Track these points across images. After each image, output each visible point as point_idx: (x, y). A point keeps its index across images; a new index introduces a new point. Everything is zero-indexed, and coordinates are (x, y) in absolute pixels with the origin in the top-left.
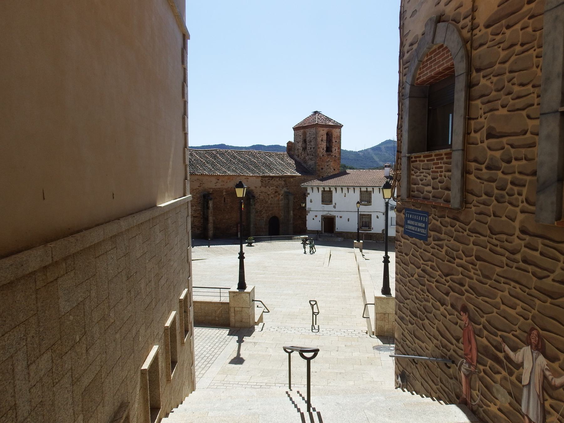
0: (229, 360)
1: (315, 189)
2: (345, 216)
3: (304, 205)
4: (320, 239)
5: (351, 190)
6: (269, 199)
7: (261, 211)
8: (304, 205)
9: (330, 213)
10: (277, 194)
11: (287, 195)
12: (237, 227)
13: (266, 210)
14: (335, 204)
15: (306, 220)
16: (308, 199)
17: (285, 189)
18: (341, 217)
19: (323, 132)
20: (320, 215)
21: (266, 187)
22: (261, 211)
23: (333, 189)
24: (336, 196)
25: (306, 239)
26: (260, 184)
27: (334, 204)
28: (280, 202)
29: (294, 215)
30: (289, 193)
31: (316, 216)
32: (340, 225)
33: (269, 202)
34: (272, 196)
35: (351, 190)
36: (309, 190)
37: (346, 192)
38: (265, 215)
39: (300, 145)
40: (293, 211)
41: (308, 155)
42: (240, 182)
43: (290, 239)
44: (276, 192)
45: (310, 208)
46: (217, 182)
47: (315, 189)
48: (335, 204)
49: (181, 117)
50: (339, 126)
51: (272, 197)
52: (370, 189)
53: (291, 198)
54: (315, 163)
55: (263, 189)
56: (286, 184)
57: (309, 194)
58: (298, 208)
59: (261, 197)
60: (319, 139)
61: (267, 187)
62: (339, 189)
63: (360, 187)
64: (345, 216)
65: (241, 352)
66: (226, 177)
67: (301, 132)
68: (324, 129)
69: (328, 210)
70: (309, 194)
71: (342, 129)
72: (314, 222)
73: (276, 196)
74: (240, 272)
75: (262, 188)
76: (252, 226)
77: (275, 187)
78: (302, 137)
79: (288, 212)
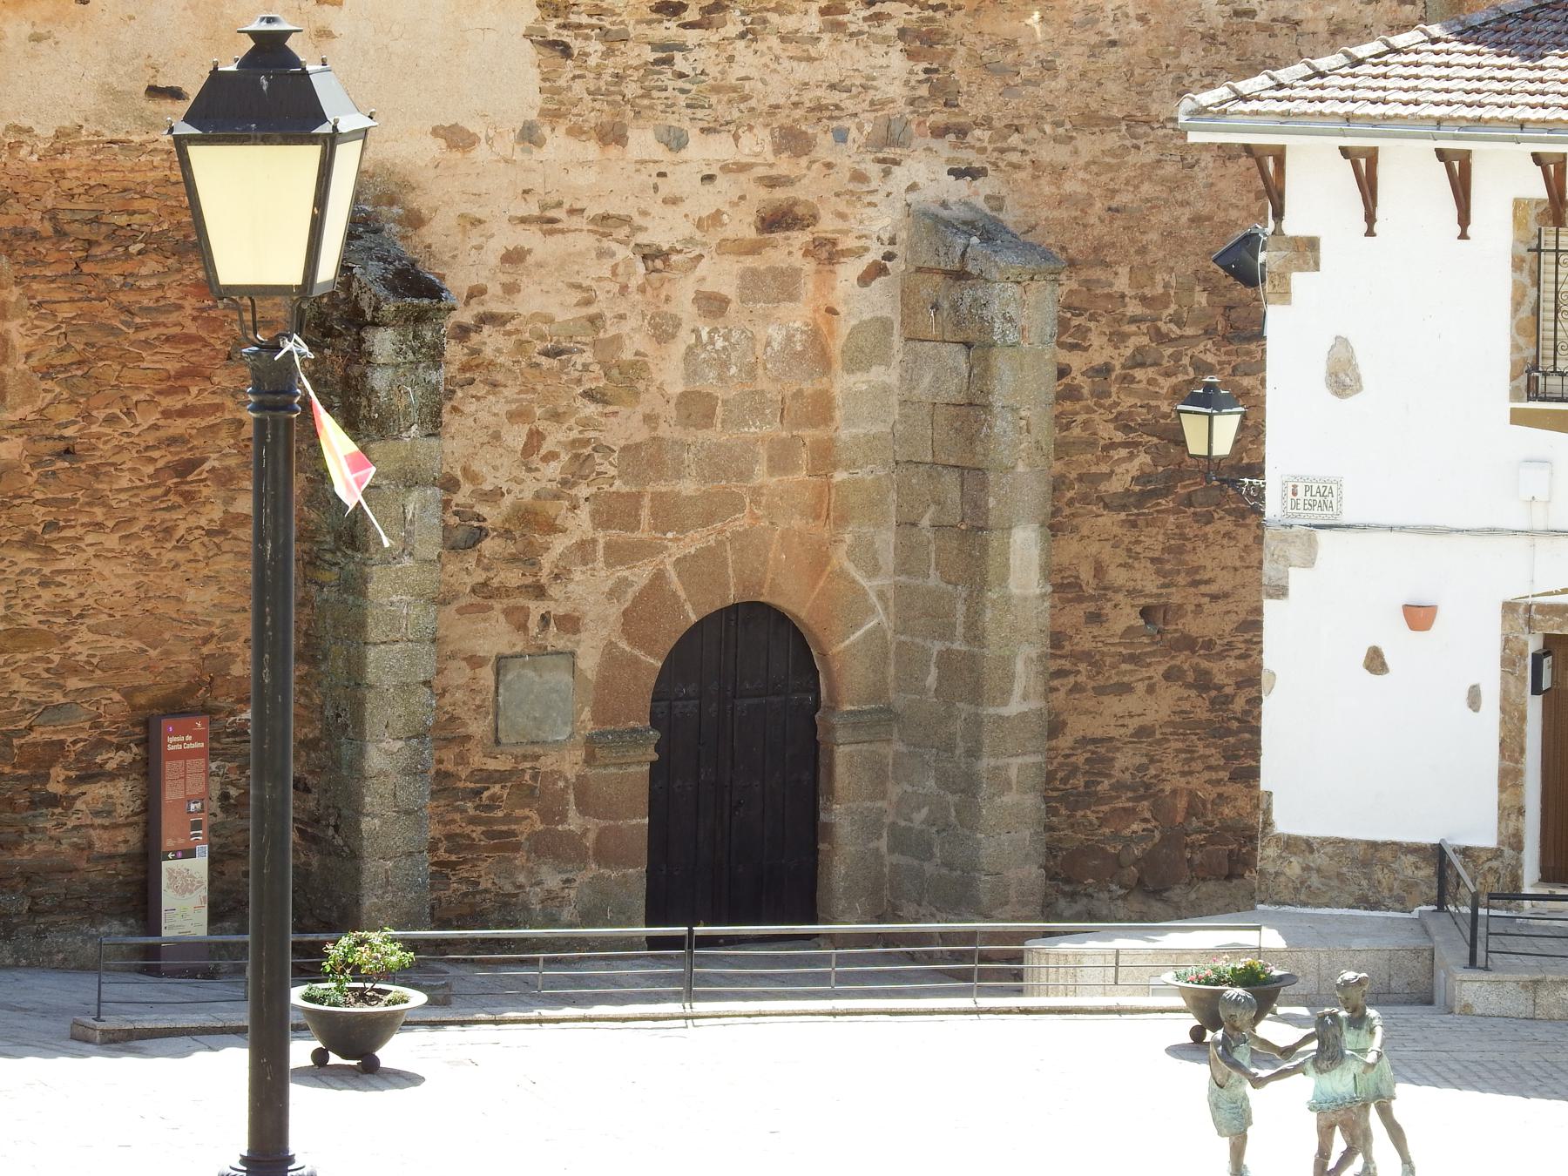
0: (1482, 689)
3: (1226, 427)
4: (1472, 989)
6: (663, 330)
7: (532, 522)
8: (1226, 427)
10: (789, 250)
11: (953, 262)
12: (149, 770)
15: (1252, 680)
16: (1293, 333)
17: (925, 174)
21: (612, 135)
22: (532, 522)
25: (1263, 990)
28: (844, 383)
29: (1064, 586)
30: (989, 231)
31: (1419, 616)
33: (670, 376)
34: (721, 275)
36: (1316, 195)
38: (592, 594)
40: (1054, 528)
42: (270, 49)
43: (993, 969)
44: (777, 220)
45: (1324, 493)
51: (713, 305)
53: (1023, 309)
55: (569, 164)
56: (944, 93)
58: (1125, 473)
59: (543, 301)
61: (643, 142)
65: (1225, 1144)
70: (1307, 250)
73: (784, 285)
75: (558, 145)
76: (383, 753)
77: (756, 145)
79: (972, 540)
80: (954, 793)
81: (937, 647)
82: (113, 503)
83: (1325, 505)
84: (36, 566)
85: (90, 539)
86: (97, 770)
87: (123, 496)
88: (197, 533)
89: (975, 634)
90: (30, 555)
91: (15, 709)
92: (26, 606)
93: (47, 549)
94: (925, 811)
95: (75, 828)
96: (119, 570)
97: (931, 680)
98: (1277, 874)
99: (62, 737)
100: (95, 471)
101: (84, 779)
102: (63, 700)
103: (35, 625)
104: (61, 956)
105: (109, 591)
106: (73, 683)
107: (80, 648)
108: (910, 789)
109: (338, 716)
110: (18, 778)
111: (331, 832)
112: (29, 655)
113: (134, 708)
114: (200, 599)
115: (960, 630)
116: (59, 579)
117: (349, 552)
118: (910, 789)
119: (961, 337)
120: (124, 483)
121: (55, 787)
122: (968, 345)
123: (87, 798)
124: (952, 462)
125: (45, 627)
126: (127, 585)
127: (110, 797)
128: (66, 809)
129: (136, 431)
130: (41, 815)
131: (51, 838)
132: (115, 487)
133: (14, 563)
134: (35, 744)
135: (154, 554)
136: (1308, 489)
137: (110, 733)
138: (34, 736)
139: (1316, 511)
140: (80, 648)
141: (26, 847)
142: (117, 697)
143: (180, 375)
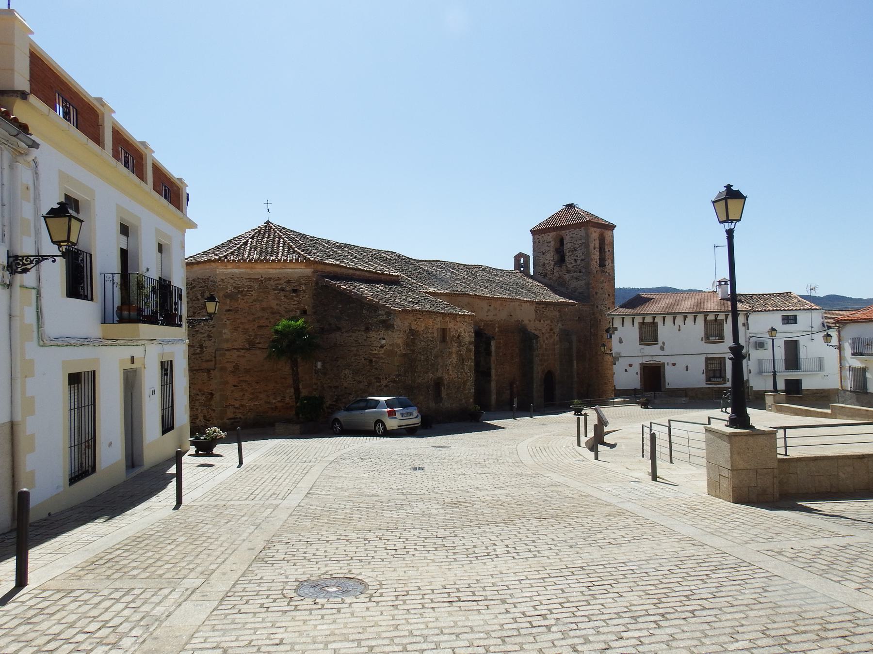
1: (628, 321)
2: (682, 362)
4: (656, 401)
5: (690, 318)
9: (655, 358)
13: (541, 361)
14: (664, 343)
16: (615, 337)
18: (674, 365)
19: (595, 234)
20: (637, 363)
23: (658, 319)
24: (665, 331)
26: (533, 316)
27: (660, 344)
31: (631, 365)
32: (673, 378)
35: (690, 318)
36: (617, 323)
37: (682, 324)
39: (549, 258)
41: (568, 271)
45: (620, 353)
46: (489, 310)
47: (628, 321)
48: (664, 343)
49: (42, 295)
50: (612, 227)
52: (721, 317)
54: (588, 284)
57: (616, 329)
60: (592, 246)
62: (669, 319)
63: (706, 314)
64: (682, 362)
66: (499, 302)
67: (550, 237)
68: (596, 229)
69: (652, 354)
70: (616, 329)
71: (615, 231)
72: (626, 375)
74: (79, 479)
77: (549, 322)
78: (553, 243)
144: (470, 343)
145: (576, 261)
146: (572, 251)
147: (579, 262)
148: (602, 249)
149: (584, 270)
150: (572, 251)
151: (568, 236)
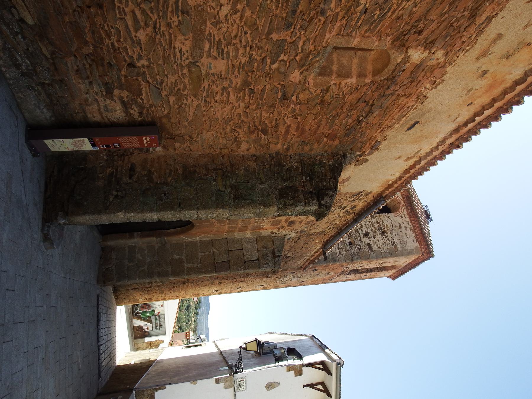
45: (243, 387)
80: (148, 269)
81: (184, 258)
82: (256, 111)
83: (240, 388)
84: (233, 85)
85: (242, 104)
86: (128, 106)
87: (258, 114)
88: (237, 135)
89: (191, 271)
90: (239, 84)
91: (158, 77)
92: (213, 82)
93: (241, 90)
94: (141, 258)
95: (96, 100)
96: (225, 113)
97: (176, 257)
98: (144, 395)
99: (144, 95)
100: (273, 106)
101: (123, 103)
102: (163, 94)
103: (203, 86)
104: (22, 96)
105: (216, 110)
106: (172, 99)
107: (189, 101)
108: (146, 252)
109: (165, 194)
110: (119, 78)
111: (115, 193)
112: (187, 83)
113: (160, 118)
114: (209, 135)
115: (190, 266)
116: (225, 94)
117: (232, 197)
118: (146, 252)
119: (260, 257)
120: (264, 114)
121: (116, 92)
122: (258, 259)
123: (113, 103)
124: (230, 258)
125: (202, 89)
126: (218, 115)
127: (115, 111)
128: (106, 96)
129: (286, 118)
130: (100, 87)
131: (88, 90)
132: (263, 111)
133: (236, 77)
134: (139, 85)
135: (231, 123)
136: (243, 383)
137: (148, 110)
138: (143, 84)
139: (238, 386)
140: (189, 101)
141: (80, 81)
142: (165, 113)
143: (303, 129)
144: (114, 89)
145: (366, 235)
146: (380, 228)
147: (365, 240)
148: (371, 270)
149: (354, 250)
150: (380, 228)
151: (399, 219)
